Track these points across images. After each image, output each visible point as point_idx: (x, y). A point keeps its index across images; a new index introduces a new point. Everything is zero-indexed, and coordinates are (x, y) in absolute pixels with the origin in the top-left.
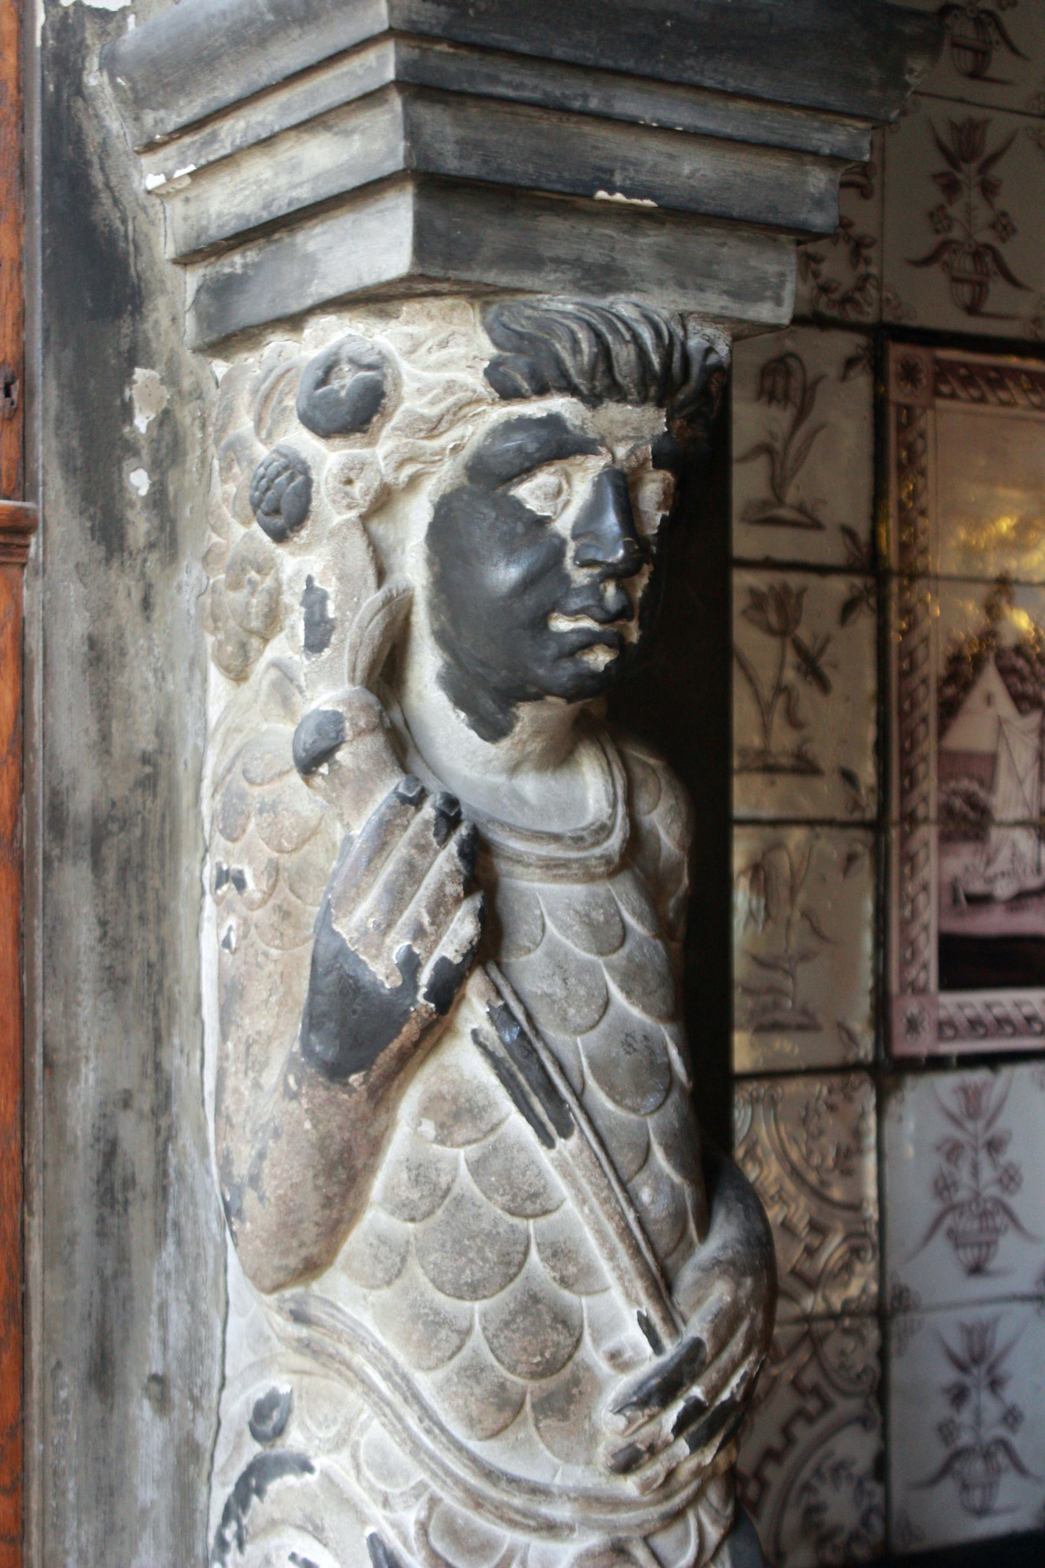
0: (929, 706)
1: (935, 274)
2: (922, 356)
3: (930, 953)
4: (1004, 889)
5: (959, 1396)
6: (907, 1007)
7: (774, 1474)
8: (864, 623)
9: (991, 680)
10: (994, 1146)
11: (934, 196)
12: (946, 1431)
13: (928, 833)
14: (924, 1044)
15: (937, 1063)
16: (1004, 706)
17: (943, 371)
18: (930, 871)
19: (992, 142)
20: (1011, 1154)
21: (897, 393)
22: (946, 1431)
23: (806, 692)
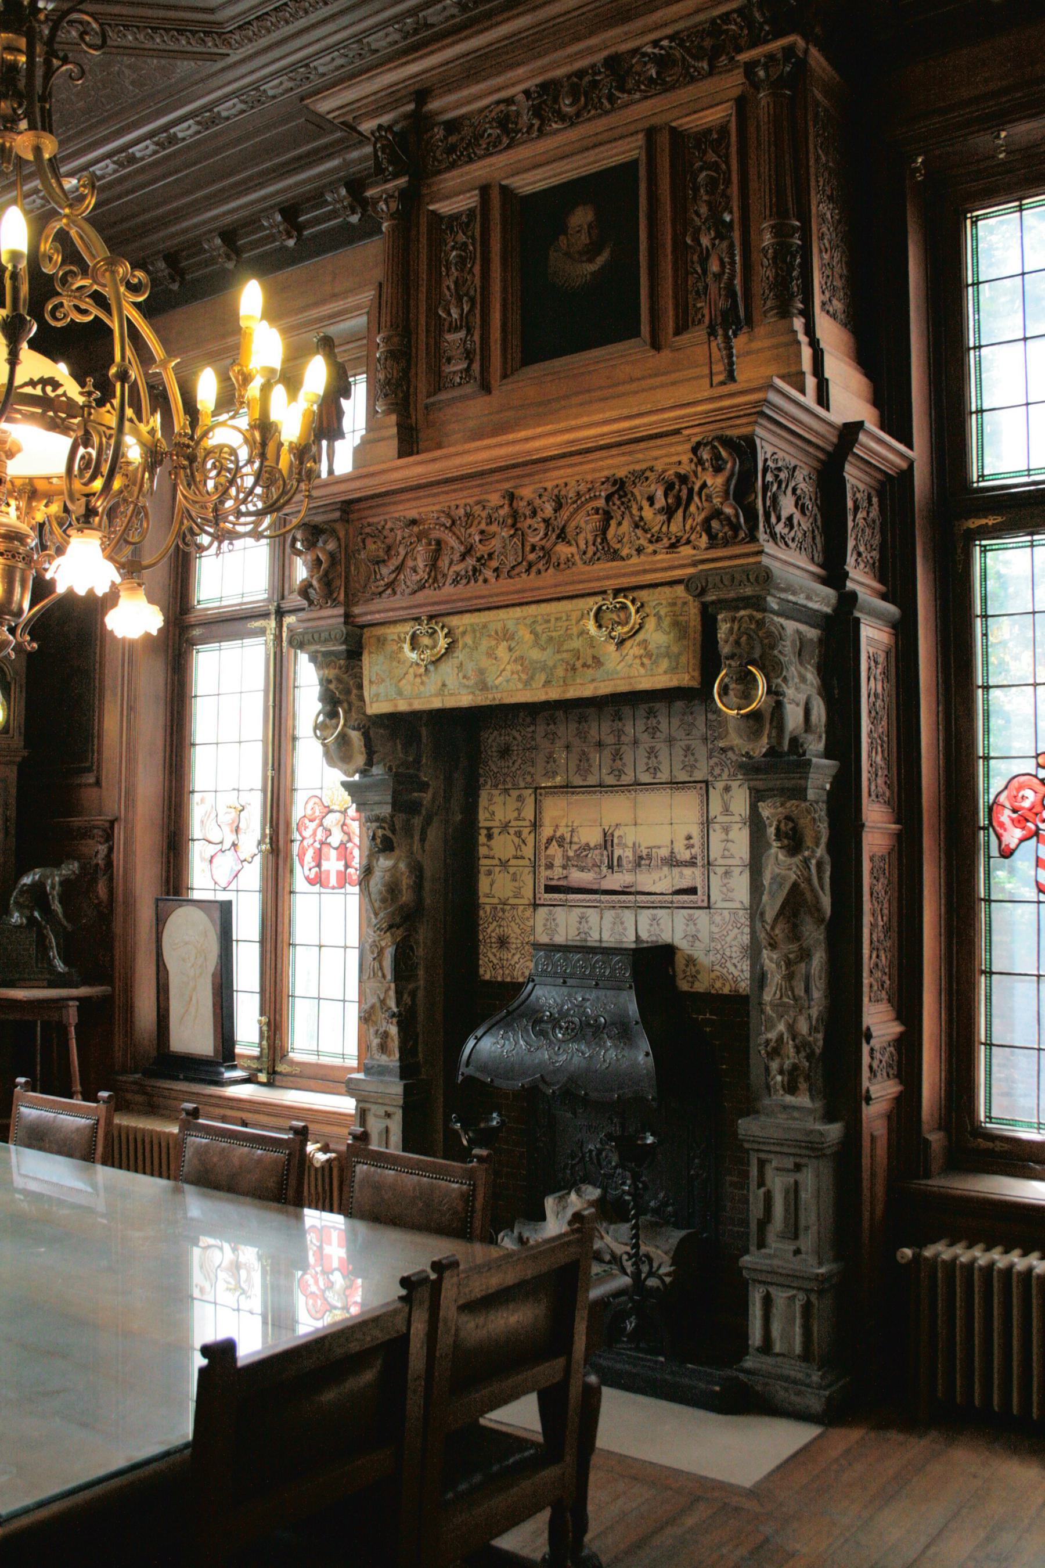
0: (543, 847)
1: (612, 776)
2: (543, 791)
3: (543, 887)
4: (556, 877)
5: (687, 966)
6: (538, 896)
7: (517, 966)
8: (533, 835)
9: (554, 842)
10: (554, 920)
11: (646, 760)
12: (684, 972)
13: (543, 868)
14: (542, 902)
15: (544, 905)
16: (557, 847)
17: (547, 793)
18: (542, 874)
19: (657, 748)
20: (625, 924)
21: (539, 797)
22: (684, 972)
23: (523, 846)
